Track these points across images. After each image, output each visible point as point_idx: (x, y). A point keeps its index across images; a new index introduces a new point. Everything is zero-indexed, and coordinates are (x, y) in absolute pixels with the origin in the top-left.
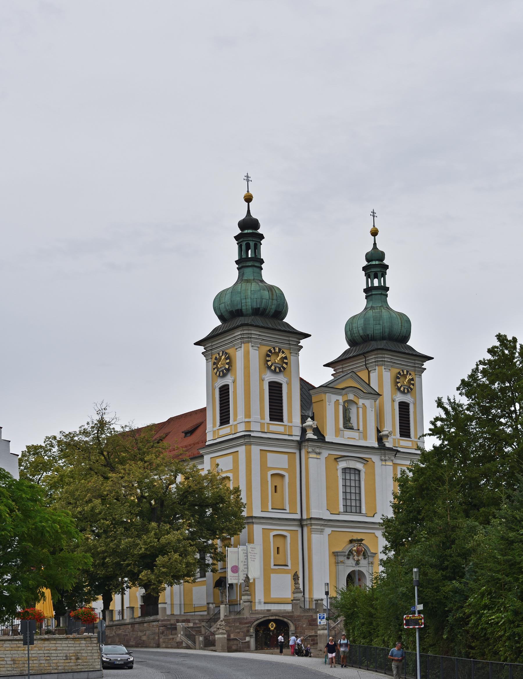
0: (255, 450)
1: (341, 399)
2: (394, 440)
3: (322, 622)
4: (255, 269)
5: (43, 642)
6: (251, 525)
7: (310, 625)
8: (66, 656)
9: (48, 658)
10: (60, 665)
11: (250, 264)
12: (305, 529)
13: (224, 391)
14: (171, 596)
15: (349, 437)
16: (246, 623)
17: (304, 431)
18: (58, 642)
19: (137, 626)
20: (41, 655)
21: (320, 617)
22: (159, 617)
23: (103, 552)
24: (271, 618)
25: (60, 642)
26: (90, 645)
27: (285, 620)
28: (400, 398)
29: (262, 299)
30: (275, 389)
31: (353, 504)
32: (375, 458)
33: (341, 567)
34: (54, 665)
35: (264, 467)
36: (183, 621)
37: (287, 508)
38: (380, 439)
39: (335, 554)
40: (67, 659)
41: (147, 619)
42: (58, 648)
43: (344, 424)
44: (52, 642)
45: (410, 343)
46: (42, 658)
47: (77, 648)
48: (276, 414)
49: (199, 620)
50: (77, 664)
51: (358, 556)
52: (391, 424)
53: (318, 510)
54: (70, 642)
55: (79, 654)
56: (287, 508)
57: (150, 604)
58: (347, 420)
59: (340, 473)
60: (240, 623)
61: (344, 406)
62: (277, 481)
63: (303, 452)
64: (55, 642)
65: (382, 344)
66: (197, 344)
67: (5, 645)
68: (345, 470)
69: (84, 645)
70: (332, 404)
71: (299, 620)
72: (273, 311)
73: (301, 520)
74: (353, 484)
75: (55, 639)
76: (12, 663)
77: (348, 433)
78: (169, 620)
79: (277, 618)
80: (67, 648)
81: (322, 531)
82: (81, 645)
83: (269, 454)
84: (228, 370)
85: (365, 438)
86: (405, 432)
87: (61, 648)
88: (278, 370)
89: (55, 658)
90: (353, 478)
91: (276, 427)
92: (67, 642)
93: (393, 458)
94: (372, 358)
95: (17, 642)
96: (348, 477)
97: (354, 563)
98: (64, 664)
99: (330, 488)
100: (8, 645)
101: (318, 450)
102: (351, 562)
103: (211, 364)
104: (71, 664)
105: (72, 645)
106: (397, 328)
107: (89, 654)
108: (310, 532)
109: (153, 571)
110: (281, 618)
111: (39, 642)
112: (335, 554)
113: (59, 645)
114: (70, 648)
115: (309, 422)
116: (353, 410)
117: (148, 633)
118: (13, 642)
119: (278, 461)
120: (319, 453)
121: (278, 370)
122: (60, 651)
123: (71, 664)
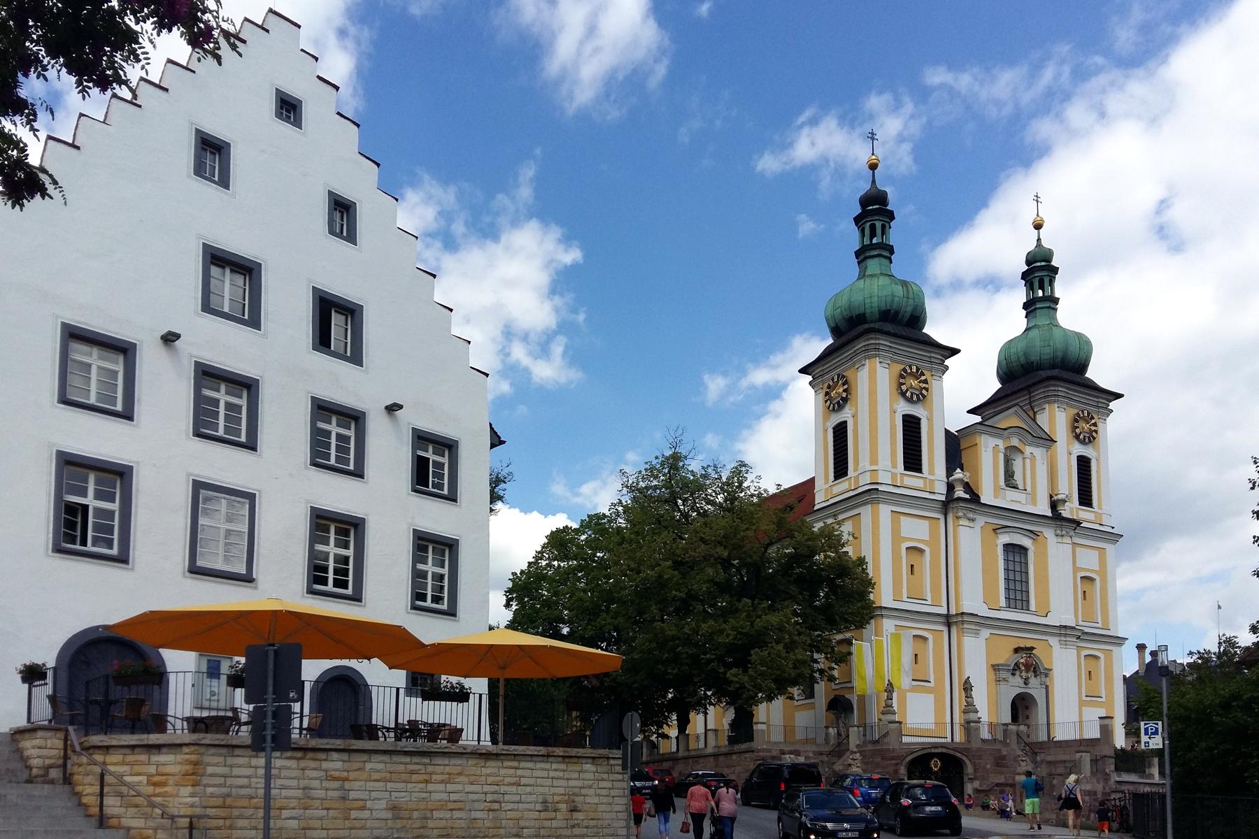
0: (885, 510)
1: (1001, 444)
2: (1071, 509)
3: (1151, 742)
4: (883, 260)
5: (482, 762)
6: (879, 619)
7: (998, 765)
8: (545, 802)
9: (496, 806)
10: (527, 824)
11: (875, 253)
12: (954, 629)
13: (840, 432)
14: (771, 716)
15: (1011, 500)
16: (892, 759)
17: (950, 487)
18: (523, 764)
19: (721, 759)
20: (472, 797)
21: (1146, 730)
22: (754, 745)
23: (674, 638)
24: (933, 751)
25: (530, 765)
26: (605, 776)
27: (958, 755)
28: (1079, 449)
29: (893, 296)
30: (911, 427)
31: (1017, 594)
32: (1048, 533)
33: (1003, 687)
34: (511, 823)
35: (897, 537)
36: (791, 753)
37: (929, 597)
38: (1054, 505)
39: (996, 668)
40: (546, 810)
41: (737, 747)
42: (523, 781)
43: (1006, 480)
44: (507, 764)
45: (1091, 374)
46: (476, 805)
47: (572, 783)
48: (913, 461)
49: (814, 753)
50: (571, 823)
51: (1027, 671)
52: (1068, 485)
53: (972, 600)
54: (555, 766)
55: (577, 799)
56: (929, 597)
57: (743, 728)
58: (1009, 475)
59: (1000, 550)
60: (883, 758)
61: (1006, 456)
62: (915, 559)
63: (950, 517)
64: (515, 764)
65: (1055, 372)
66: (804, 371)
67: (369, 766)
68: (1009, 547)
69: (591, 776)
70: (990, 450)
71: (980, 757)
72: (908, 315)
73: (948, 616)
74: (1018, 568)
75: (515, 756)
76: (389, 815)
77: (1011, 494)
78: (769, 751)
79: (944, 750)
80: (549, 782)
81: (977, 633)
82: (583, 776)
83: (903, 518)
84: (845, 400)
85: (1034, 503)
86: (1085, 498)
87: (532, 781)
88: (915, 398)
89: (515, 806)
90: (1017, 559)
91: (912, 480)
92: (547, 766)
93: (1072, 533)
94: (1038, 393)
95: (407, 759)
96: (1011, 558)
97: (1021, 681)
98: (537, 824)
99: (988, 572)
100: (381, 766)
101: (971, 515)
102: (1017, 680)
103: (821, 396)
104: (555, 824)
105: (561, 774)
106: (1074, 350)
107: (605, 800)
108: (962, 632)
109: (745, 671)
110: (952, 752)
111: (471, 762)
112: (996, 668)
113: (528, 773)
114: (556, 783)
115: (958, 474)
116: (1017, 466)
117: (738, 769)
118: (396, 758)
119: (917, 529)
120: (973, 520)
121: (915, 398)
122: (528, 789)
123: (555, 824)
